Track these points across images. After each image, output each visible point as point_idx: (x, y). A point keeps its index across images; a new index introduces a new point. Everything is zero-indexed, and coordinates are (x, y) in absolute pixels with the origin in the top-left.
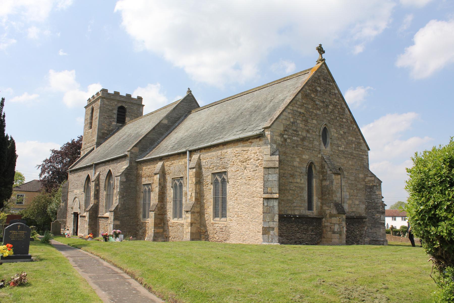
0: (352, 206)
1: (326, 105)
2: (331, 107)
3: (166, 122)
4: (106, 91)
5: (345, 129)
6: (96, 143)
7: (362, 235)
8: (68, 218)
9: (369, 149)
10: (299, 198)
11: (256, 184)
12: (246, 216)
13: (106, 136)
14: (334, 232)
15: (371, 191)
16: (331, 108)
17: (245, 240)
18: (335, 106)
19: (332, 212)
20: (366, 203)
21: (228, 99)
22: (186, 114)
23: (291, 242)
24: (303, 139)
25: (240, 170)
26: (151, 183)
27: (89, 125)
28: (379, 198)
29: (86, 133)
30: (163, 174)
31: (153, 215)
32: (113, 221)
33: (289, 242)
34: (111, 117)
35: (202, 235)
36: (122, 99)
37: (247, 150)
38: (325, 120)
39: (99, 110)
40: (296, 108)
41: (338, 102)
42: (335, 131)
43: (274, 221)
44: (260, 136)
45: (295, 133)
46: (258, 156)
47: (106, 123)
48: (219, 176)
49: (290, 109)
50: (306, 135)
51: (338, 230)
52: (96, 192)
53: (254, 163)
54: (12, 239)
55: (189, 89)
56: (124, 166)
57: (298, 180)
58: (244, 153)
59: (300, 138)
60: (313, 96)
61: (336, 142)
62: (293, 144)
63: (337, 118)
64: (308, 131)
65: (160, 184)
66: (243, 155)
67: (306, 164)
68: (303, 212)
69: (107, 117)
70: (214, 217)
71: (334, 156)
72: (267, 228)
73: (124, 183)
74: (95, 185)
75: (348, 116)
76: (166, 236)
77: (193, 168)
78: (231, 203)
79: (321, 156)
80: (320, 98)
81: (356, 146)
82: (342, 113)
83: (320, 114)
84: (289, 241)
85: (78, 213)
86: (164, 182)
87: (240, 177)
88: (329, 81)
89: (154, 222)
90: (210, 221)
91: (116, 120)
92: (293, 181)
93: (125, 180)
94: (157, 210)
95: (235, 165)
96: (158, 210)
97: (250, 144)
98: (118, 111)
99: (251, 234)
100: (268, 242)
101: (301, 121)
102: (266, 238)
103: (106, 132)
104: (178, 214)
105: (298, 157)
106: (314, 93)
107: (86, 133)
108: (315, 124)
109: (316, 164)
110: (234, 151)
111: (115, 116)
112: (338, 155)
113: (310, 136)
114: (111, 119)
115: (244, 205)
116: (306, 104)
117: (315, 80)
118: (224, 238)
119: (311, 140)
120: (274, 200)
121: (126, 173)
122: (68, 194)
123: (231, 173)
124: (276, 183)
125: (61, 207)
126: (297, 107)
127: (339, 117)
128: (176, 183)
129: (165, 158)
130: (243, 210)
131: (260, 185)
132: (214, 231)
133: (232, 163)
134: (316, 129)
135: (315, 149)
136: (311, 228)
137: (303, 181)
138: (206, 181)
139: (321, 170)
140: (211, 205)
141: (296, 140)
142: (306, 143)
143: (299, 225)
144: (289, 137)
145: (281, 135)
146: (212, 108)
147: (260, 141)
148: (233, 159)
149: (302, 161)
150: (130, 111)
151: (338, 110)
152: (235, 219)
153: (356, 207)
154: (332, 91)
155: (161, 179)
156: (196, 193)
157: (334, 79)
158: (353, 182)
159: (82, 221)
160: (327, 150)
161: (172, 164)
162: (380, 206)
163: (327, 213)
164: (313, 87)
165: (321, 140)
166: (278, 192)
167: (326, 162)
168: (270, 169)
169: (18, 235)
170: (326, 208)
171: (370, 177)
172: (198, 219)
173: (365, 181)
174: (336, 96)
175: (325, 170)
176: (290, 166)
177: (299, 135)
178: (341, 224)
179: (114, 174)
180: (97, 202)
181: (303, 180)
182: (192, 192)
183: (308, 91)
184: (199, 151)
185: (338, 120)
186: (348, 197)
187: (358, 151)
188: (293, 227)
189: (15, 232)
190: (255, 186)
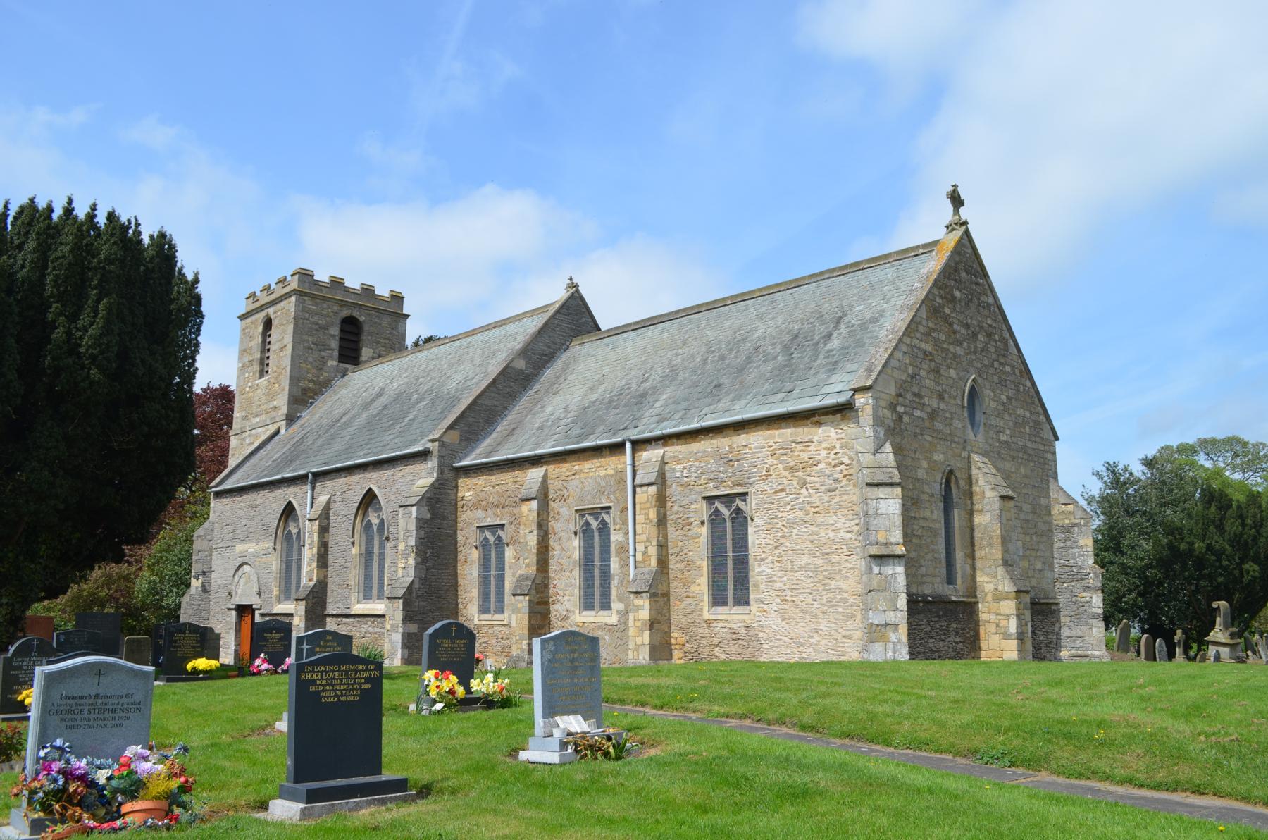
2: (981, 338)
5: (1010, 391)
6: (287, 415)
7: (1050, 642)
9: (1057, 439)
10: (930, 556)
11: (836, 522)
15: (1067, 539)
16: (982, 339)
19: (1000, 588)
21: (697, 311)
25: (788, 490)
27: (257, 367)
28: (1087, 555)
29: (247, 389)
31: (526, 604)
34: (324, 346)
40: (916, 342)
41: (994, 325)
42: (992, 394)
43: (896, 610)
44: (844, 410)
45: (917, 400)
46: (839, 455)
47: (311, 363)
48: (722, 503)
49: (908, 345)
52: (323, 549)
53: (827, 472)
56: (423, 477)
57: (928, 514)
60: (947, 311)
61: (993, 422)
63: (993, 364)
64: (941, 397)
66: (796, 453)
67: (941, 475)
70: (711, 605)
71: (991, 454)
72: (882, 625)
73: (426, 523)
75: (1015, 358)
78: (763, 568)
81: (1033, 429)
82: (1002, 352)
83: (962, 354)
85: (254, 607)
87: (789, 507)
88: (975, 276)
89: (527, 622)
90: (700, 615)
91: (336, 354)
92: (917, 516)
93: (428, 516)
94: (533, 592)
96: (537, 593)
98: (342, 330)
101: (928, 372)
102: (881, 649)
103: (311, 385)
104: (491, 600)
105: (926, 458)
107: (247, 389)
109: (958, 475)
110: (770, 444)
111: (335, 344)
112: (999, 453)
114: (323, 351)
116: (935, 330)
117: (950, 273)
121: (429, 498)
122: (211, 556)
124: (898, 520)
129: (551, 459)
130: (797, 587)
131: (847, 525)
133: (764, 473)
135: (956, 439)
136: (954, 625)
137: (938, 514)
138: (686, 516)
140: (702, 576)
143: (933, 619)
144: (907, 409)
145: (892, 407)
146: (651, 332)
147: (842, 420)
148: (766, 463)
149: (933, 466)
150: (372, 329)
152: (776, 609)
154: (982, 299)
157: (984, 267)
158: (1029, 517)
161: (574, 475)
162: (1089, 573)
163: (986, 591)
164: (947, 290)
166: (901, 541)
169: (452, 649)
170: (986, 579)
176: (910, 480)
177: (924, 405)
178: (1023, 617)
181: (935, 512)
182: (647, 544)
183: (938, 300)
184: (660, 442)
185: (996, 369)
186: (1021, 554)
188: (920, 625)
190: (833, 528)
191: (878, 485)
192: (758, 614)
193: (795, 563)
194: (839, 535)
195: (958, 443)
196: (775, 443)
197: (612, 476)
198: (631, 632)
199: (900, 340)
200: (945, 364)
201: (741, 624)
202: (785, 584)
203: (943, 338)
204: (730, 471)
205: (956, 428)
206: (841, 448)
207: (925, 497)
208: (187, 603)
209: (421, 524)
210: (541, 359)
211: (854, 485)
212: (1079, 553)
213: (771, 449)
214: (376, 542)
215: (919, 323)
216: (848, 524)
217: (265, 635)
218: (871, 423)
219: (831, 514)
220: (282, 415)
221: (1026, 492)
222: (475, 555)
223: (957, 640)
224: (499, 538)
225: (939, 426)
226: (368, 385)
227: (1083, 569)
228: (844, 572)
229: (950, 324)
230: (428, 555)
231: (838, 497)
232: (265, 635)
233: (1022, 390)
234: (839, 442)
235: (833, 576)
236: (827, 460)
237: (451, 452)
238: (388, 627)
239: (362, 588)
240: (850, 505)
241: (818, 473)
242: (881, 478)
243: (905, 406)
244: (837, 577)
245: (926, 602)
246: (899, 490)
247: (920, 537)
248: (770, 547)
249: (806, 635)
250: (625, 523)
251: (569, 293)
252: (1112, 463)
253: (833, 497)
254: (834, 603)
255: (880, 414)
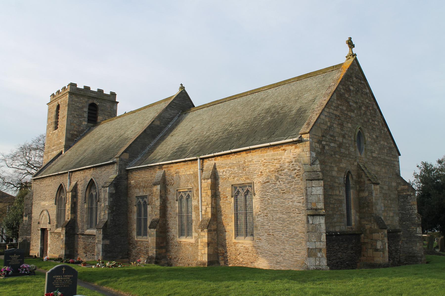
0: (387, 219)
1: (359, 106)
2: (363, 108)
3: (158, 123)
4: (75, 85)
5: (377, 133)
6: (65, 145)
7: (397, 250)
8: (32, 235)
9: (400, 155)
10: (338, 213)
12: (281, 235)
13: (76, 138)
14: (377, 250)
16: (364, 109)
17: (279, 262)
18: (367, 107)
19: (373, 227)
20: (400, 214)
22: (180, 113)
23: (332, 263)
24: (340, 145)
25: (270, 182)
26: (147, 195)
27: (53, 125)
28: (414, 209)
30: (164, 185)
31: (155, 233)
32: (102, 240)
33: (330, 263)
35: (220, 256)
36: (93, 95)
37: (279, 159)
38: (359, 123)
39: (67, 107)
41: (370, 102)
43: (321, 241)
45: (332, 138)
46: (294, 165)
49: (327, 112)
50: (343, 140)
51: (381, 247)
52: (73, 205)
53: (289, 174)
54: (56, 287)
55: (181, 85)
57: (337, 193)
58: (275, 162)
59: (337, 144)
60: (347, 96)
62: (331, 151)
63: (369, 121)
64: (344, 137)
65: (161, 197)
66: (274, 164)
68: (343, 228)
69: (76, 116)
70: (236, 235)
71: (369, 163)
72: (314, 249)
74: (71, 196)
76: (170, 257)
77: (208, 179)
78: (259, 219)
79: (357, 164)
80: (354, 99)
81: (388, 151)
82: (374, 115)
83: (354, 116)
84: (331, 262)
86: (166, 195)
87: (271, 190)
88: (360, 80)
89: (155, 241)
95: (264, 175)
97: (283, 151)
98: (89, 109)
99: (287, 255)
100: (316, 266)
101: (338, 125)
103: (75, 133)
105: (336, 166)
106: (348, 93)
107: (50, 135)
108: (350, 128)
109: (353, 173)
110: (262, 160)
111: (86, 115)
112: (372, 163)
113: (346, 141)
115: (277, 221)
116: (341, 105)
118: (250, 260)
119: (347, 146)
120: (321, 217)
121: (114, 184)
123: (258, 185)
125: (24, 222)
126: (332, 109)
127: (371, 119)
128: (182, 195)
130: (275, 228)
132: (236, 252)
133: (260, 174)
134: (352, 133)
135: (352, 157)
137: (342, 192)
139: (357, 179)
141: (334, 146)
142: (343, 150)
143: (340, 243)
144: (327, 143)
145: (319, 142)
149: (340, 170)
151: (370, 112)
152: (265, 238)
153: (390, 219)
154: (363, 90)
155: (162, 191)
156: (212, 207)
158: (387, 192)
159: (54, 239)
160: (363, 157)
162: (415, 217)
163: (366, 228)
165: (356, 146)
166: (323, 207)
167: (363, 170)
168: (313, 181)
169: (63, 280)
170: (366, 223)
171: (402, 185)
172: (215, 237)
173: (398, 189)
174: (367, 96)
175: (362, 180)
176: (329, 177)
177: (336, 140)
179: (97, 184)
180: (74, 217)
181: (341, 191)
182: (207, 206)
183: (342, 91)
185: (370, 123)
186: (383, 209)
187: (390, 156)
189: (59, 277)
191: (312, 180)
192: (257, 241)
193: (274, 217)
194: (294, 204)
195: (352, 158)
196: (265, 159)
197: (192, 174)
198: (200, 247)
199: (323, 110)
200: (346, 121)
201: (249, 245)
202: (269, 227)
203: (345, 109)
204: (244, 172)
205: (351, 151)
206: (295, 162)
207: (336, 185)
208: (22, 227)
209: (111, 195)
210: (167, 120)
211: (301, 180)
212: (410, 208)
213: (263, 162)
214: (94, 203)
215: (333, 102)
216: (299, 198)
217: (10, 256)
218: (309, 150)
219: (291, 194)
220: (63, 146)
221: (385, 180)
222: (135, 209)
223: (352, 252)
224: (145, 202)
225: (343, 150)
226: (98, 133)
227: (412, 215)
228: (296, 221)
229: (348, 102)
230: (114, 209)
231: (294, 185)
232: (10, 256)
233: (383, 132)
234: (294, 159)
235: (291, 223)
236: (288, 168)
237: (125, 163)
238: (96, 241)
239: (89, 223)
240: (299, 189)
241: (284, 174)
242: (314, 177)
243: (326, 141)
244: (294, 224)
245: (337, 235)
246: (322, 182)
247: (334, 204)
248: (263, 209)
249: (279, 251)
250: (198, 196)
251: (181, 90)
252: (424, 162)
253: (291, 185)
254: (292, 236)
255: (314, 145)
